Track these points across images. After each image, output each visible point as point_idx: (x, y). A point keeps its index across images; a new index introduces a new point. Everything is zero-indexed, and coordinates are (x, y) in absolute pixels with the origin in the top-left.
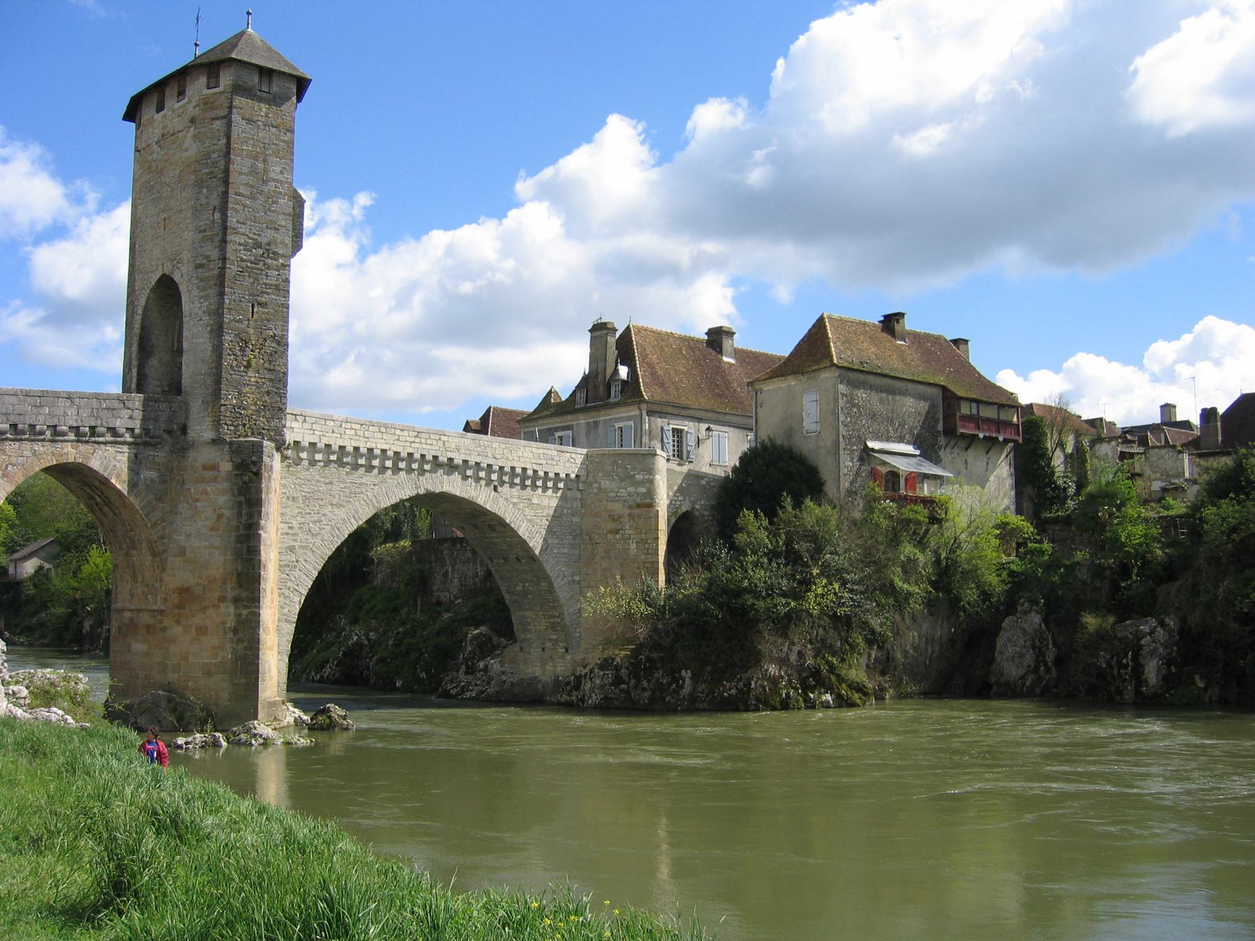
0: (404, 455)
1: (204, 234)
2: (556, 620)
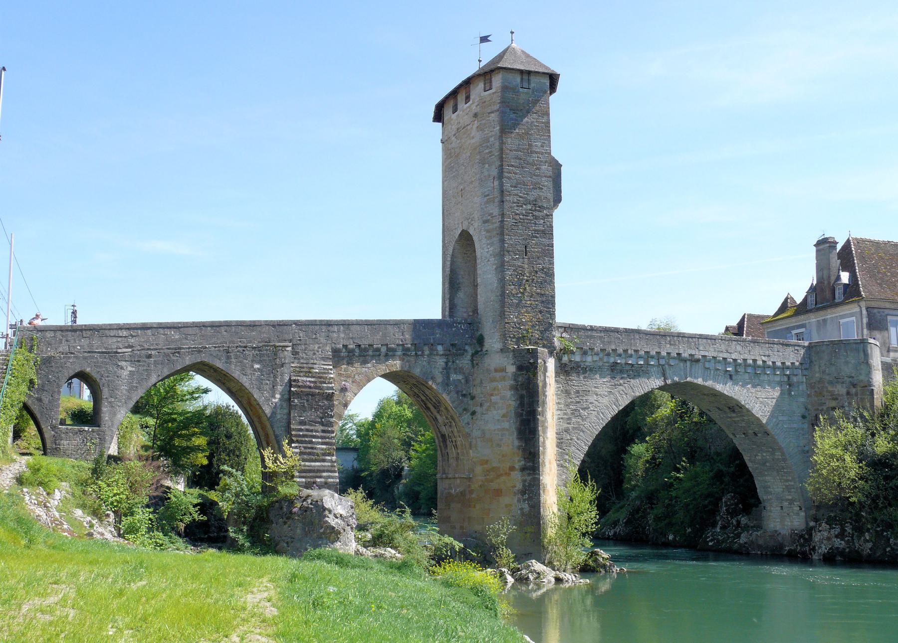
0: (653, 353)
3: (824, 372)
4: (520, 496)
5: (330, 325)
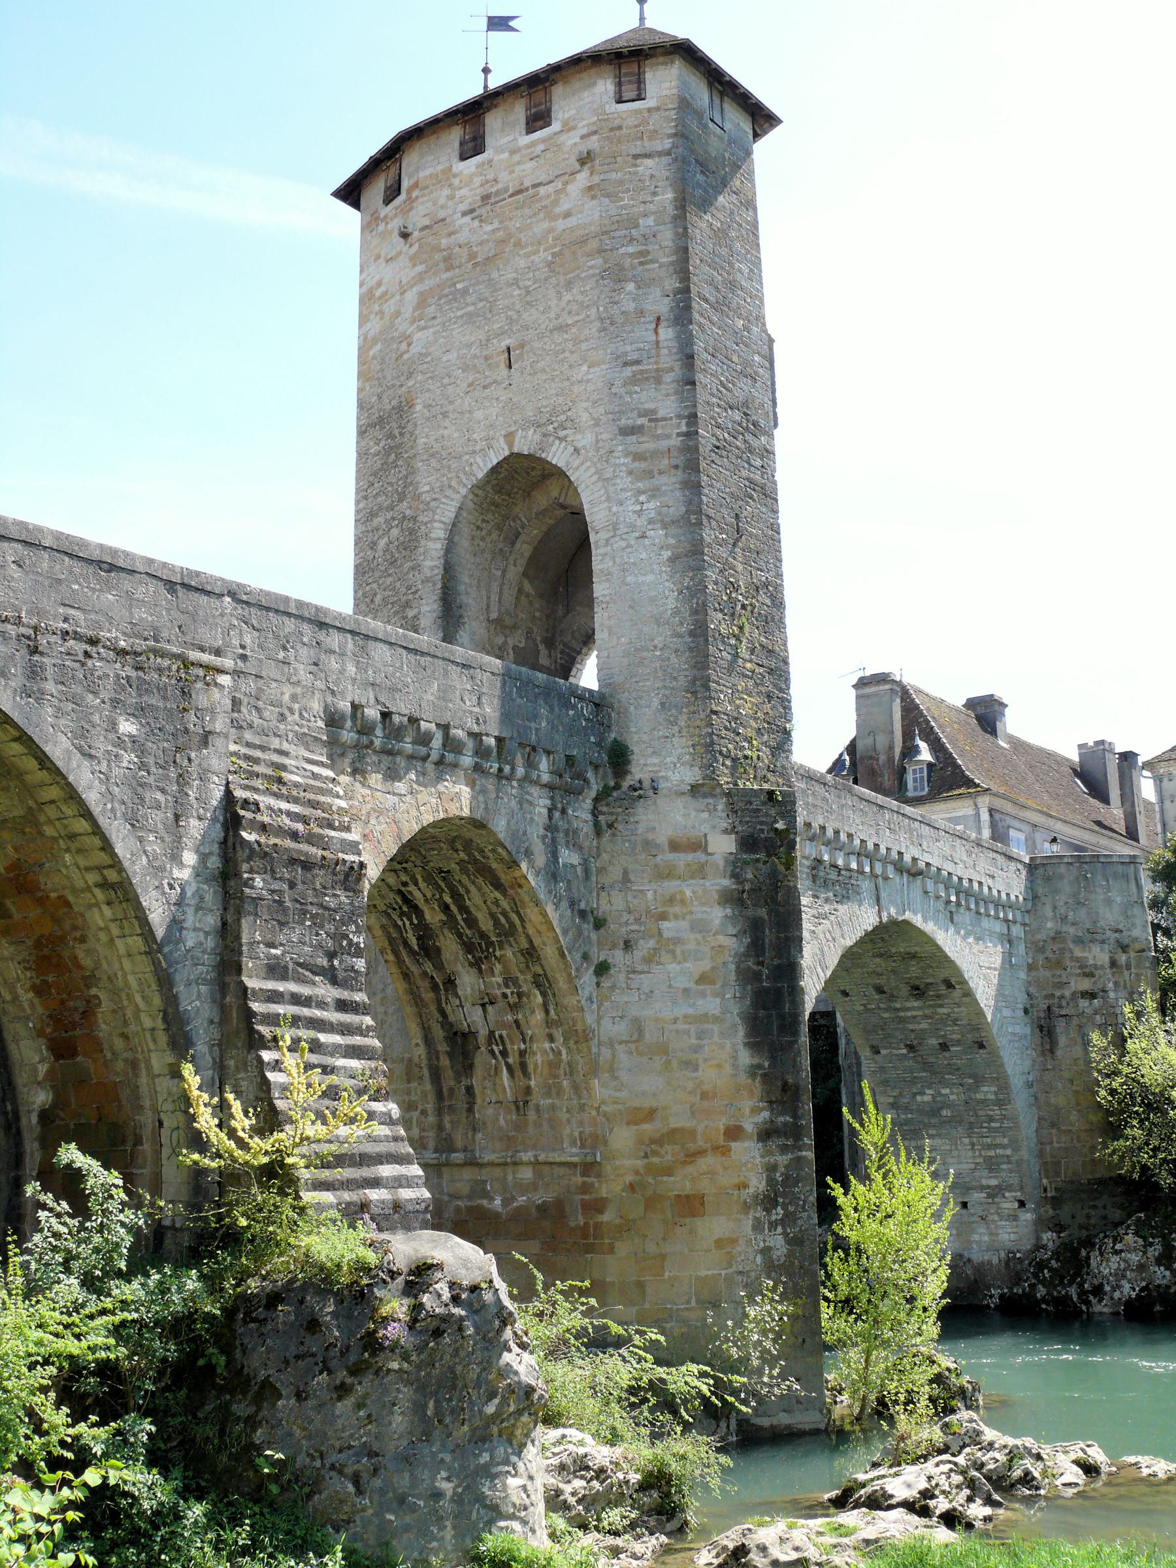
1: (634, 368)
2: (999, 1151)
3: (1064, 919)
4: (760, 1213)
5: (322, 625)
